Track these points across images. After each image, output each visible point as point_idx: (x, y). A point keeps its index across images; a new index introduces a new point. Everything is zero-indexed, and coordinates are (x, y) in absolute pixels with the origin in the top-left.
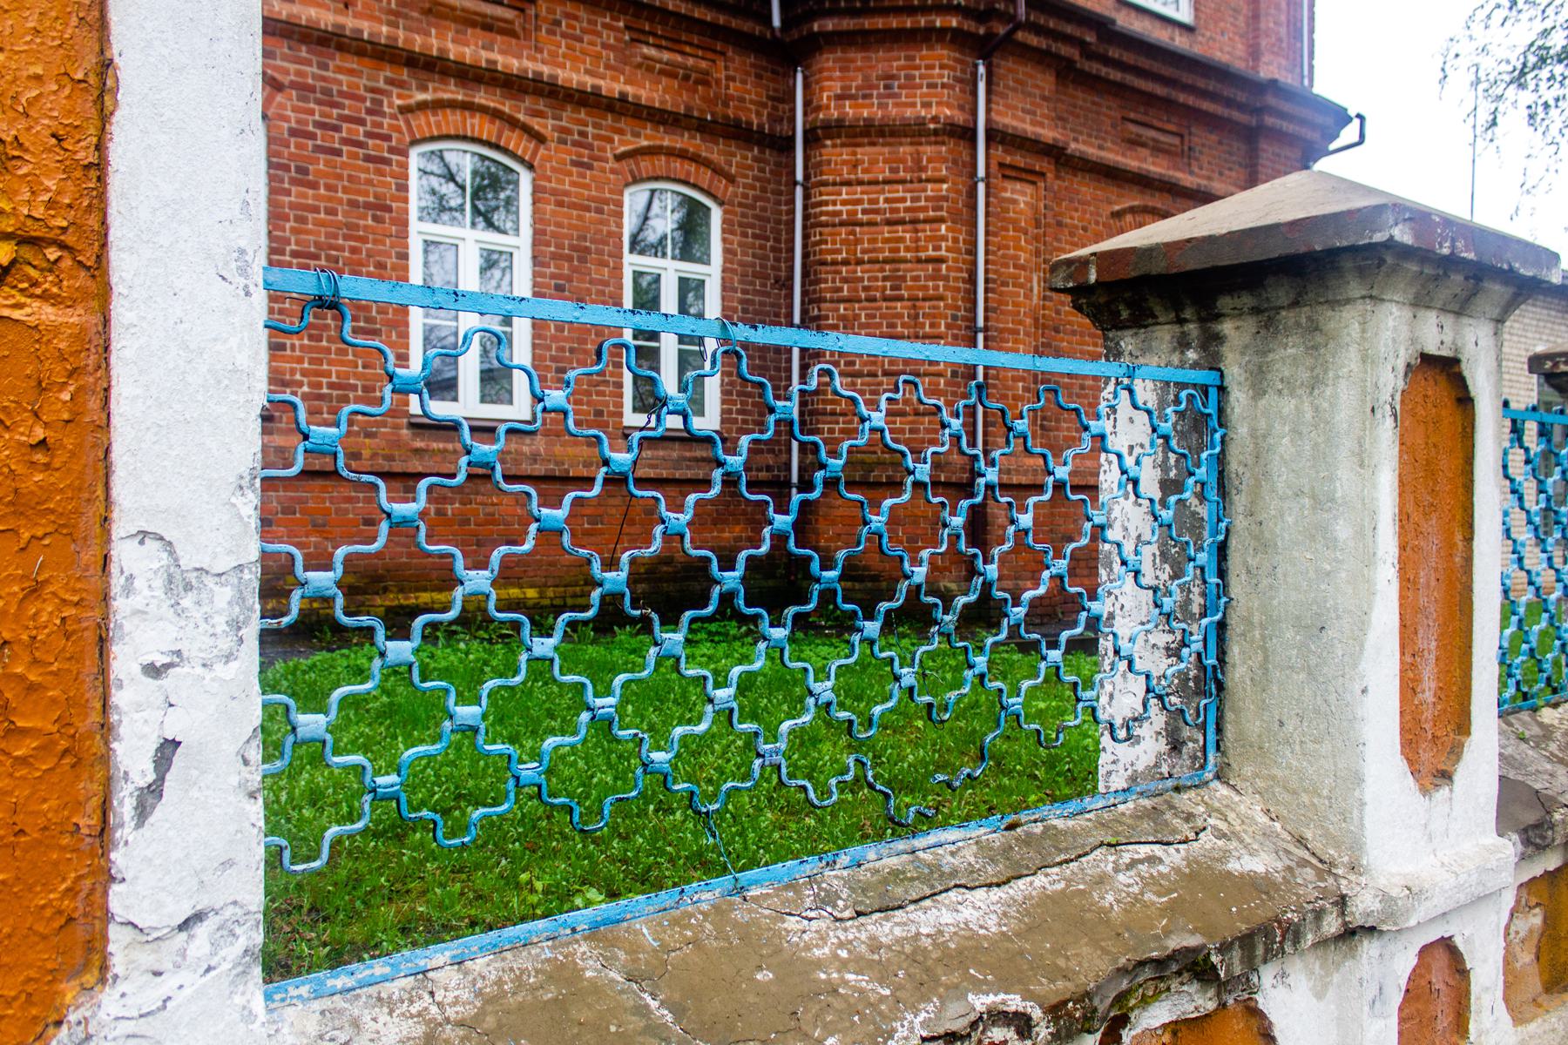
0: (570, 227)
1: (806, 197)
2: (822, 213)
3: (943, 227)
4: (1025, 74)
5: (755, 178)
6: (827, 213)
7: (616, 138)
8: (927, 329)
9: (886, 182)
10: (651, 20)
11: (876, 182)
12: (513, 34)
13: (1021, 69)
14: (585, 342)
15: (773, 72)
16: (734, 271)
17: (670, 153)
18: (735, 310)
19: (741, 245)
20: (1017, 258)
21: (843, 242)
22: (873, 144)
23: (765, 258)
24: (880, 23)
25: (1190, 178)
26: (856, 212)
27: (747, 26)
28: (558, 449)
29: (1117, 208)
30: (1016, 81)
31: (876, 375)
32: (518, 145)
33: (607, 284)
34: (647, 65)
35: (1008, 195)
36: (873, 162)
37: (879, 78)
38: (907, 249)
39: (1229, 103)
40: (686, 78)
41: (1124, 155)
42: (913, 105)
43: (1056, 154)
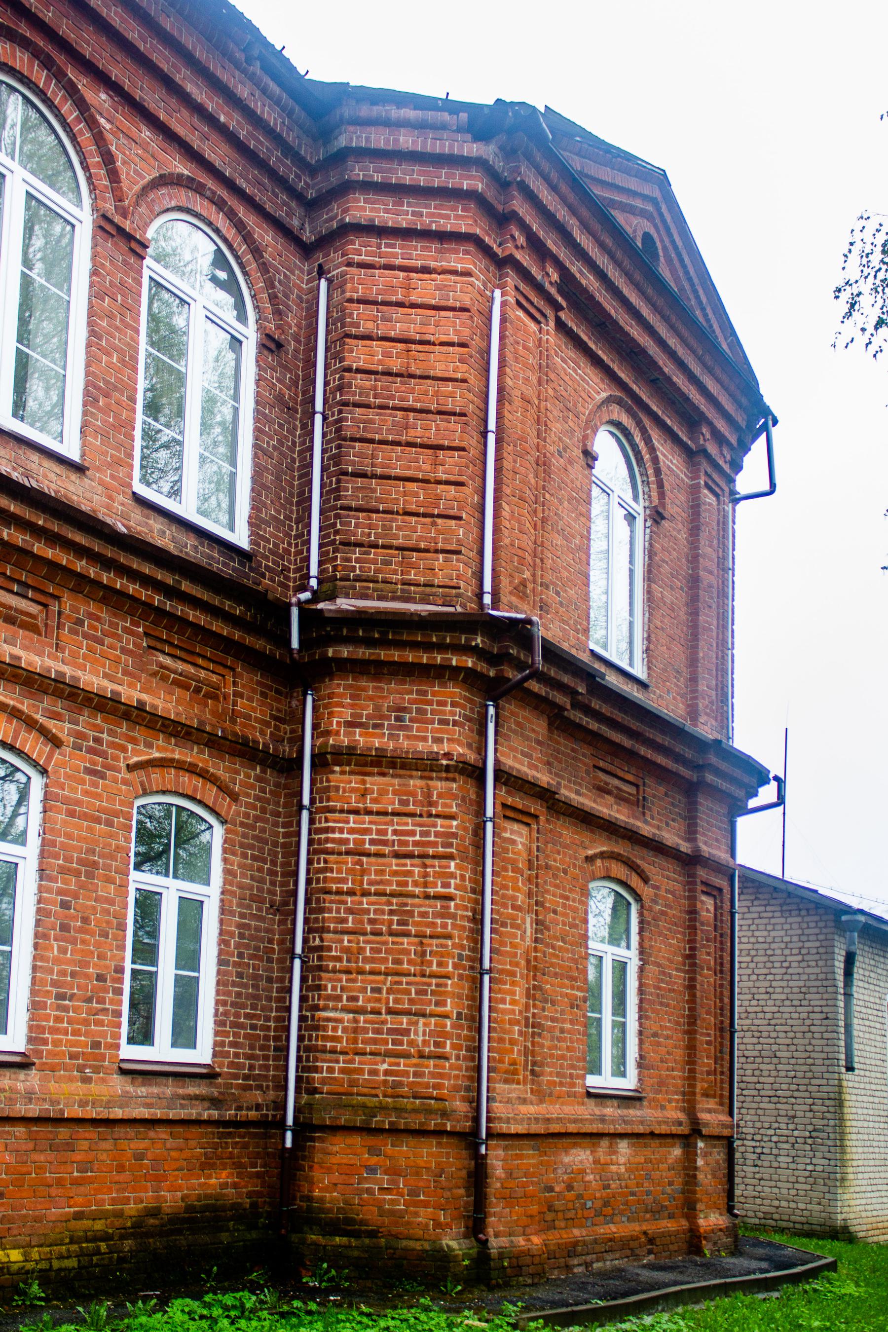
0: (80, 839)
1: (312, 821)
2: (327, 840)
3: (453, 864)
4: (524, 718)
5: (257, 798)
6: (333, 840)
7: (130, 746)
8: (434, 967)
9: (395, 814)
10: (169, 628)
11: (386, 814)
12: (35, 629)
13: (522, 713)
14: (86, 965)
15: (278, 692)
16: (233, 893)
17: (180, 766)
18: (232, 934)
19: (240, 866)
20: (515, 898)
21: (349, 871)
22: (383, 774)
23: (262, 881)
24: (395, 655)
25: (647, 828)
26: (363, 842)
27: (259, 644)
28: (52, 1085)
29: (590, 852)
30: (518, 724)
31: (380, 1013)
32: (33, 748)
33: (112, 902)
34: (162, 674)
35: (507, 835)
36: (383, 792)
37: (389, 709)
38: (415, 883)
39: (678, 758)
40: (198, 690)
41: (595, 801)
42: (425, 739)
43: (546, 796)
